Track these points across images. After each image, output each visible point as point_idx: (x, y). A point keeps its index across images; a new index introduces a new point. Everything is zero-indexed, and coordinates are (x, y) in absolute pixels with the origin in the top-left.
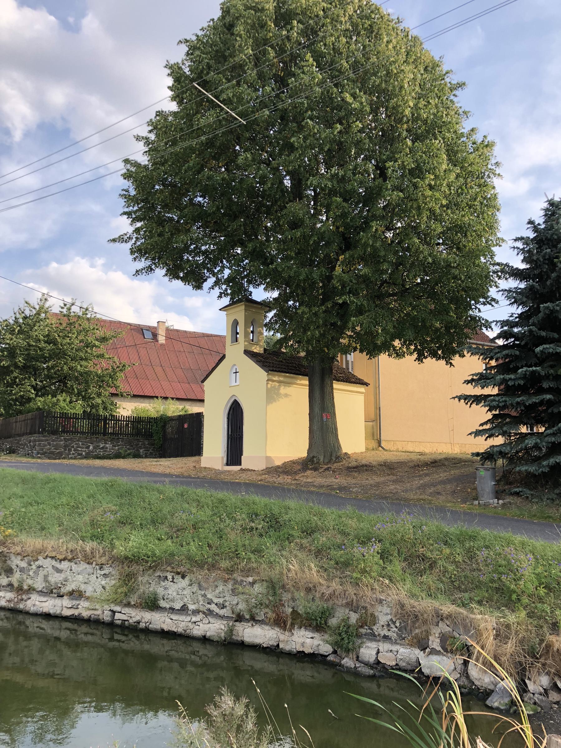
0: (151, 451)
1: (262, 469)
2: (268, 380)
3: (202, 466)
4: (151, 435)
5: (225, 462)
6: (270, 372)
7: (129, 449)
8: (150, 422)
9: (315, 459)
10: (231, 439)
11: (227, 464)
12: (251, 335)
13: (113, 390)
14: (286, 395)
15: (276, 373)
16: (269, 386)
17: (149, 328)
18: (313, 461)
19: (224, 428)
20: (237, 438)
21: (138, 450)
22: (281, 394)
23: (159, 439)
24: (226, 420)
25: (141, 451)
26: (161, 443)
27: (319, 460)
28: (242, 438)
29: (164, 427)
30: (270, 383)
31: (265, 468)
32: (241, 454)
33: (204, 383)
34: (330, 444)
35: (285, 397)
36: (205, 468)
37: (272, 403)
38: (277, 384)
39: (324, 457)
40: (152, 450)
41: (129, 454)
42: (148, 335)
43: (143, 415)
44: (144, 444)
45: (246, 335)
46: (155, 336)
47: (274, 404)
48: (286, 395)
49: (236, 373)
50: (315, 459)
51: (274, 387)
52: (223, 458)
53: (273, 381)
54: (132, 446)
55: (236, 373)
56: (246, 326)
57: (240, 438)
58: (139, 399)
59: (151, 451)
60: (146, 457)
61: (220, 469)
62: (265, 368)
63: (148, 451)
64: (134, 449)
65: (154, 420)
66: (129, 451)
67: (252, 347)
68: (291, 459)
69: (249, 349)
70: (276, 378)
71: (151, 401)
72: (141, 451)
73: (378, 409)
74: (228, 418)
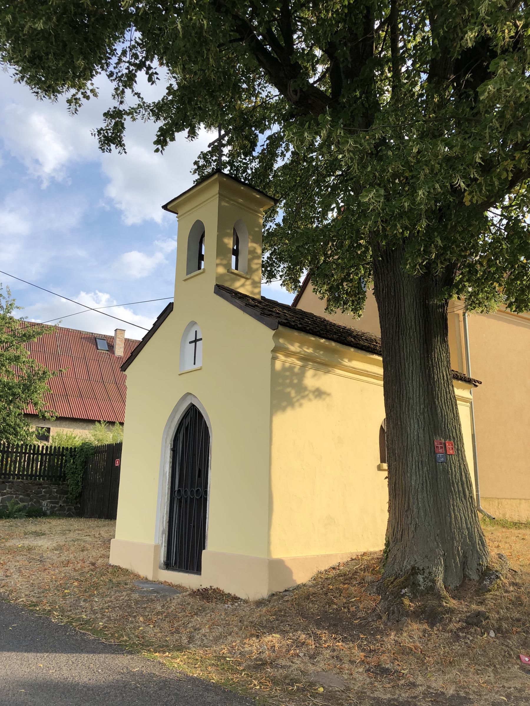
0: (61, 503)
1: (258, 597)
2: (275, 350)
3: (113, 561)
4: (63, 477)
5: (162, 558)
6: (281, 328)
7: (22, 500)
8: (63, 455)
9: (420, 578)
10: (180, 501)
11: (168, 565)
12: (234, 257)
13: (30, 409)
14: (319, 393)
15: (296, 333)
16: (278, 365)
17: (104, 338)
18: (415, 585)
19: (164, 474)
20: (192, 500)
21: (38, 502)
22: (305, 389)
23: (77, 484)
24: (168, 454)
25: (44, 503)
26: (79, 490)
27: (434, 581)
28: (206, 500)
29: (85, 463)
30: (281, 357)
31: (263, 593)
32: (202, 546)
33: (128, 372)
34: (460, 529)
35: (316, 397)
36: (118, 568)
37: (284, 409)
38: (299, 363)
39: (446, 568)
40: (64, 502)
41: (20, 510)
42: (102, 345)
43: (65, 445)
44: (50, 492)
45: (221, 250)
46: (111, 348)
47: (289, 412)
48: (319, 393)
49: (196, 341)
50: (420, 578)
51: (291, 369)
52: (157, 548)
53: (289, 354)
54: (28, 495)
55: (196, 341)
56: (221, 235)
57: (199, 501)
58: (81, 424)
59: (61, 503)
60: (54, 514)
61: (150, 578)
62: (268, 319)
63: (57, 503)
64: (31, 500)
65: (71, 452)
66: (21, 504)
67: (234, 280)
68: (334, 563)
69: (227, 284)
70: (295, 348)
71: (92, 426)
72: (44, 503)
73: (474, 434)
74: (174, 450)
